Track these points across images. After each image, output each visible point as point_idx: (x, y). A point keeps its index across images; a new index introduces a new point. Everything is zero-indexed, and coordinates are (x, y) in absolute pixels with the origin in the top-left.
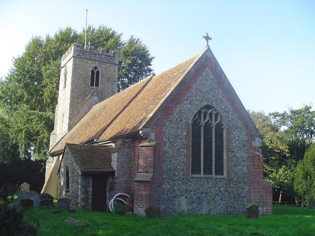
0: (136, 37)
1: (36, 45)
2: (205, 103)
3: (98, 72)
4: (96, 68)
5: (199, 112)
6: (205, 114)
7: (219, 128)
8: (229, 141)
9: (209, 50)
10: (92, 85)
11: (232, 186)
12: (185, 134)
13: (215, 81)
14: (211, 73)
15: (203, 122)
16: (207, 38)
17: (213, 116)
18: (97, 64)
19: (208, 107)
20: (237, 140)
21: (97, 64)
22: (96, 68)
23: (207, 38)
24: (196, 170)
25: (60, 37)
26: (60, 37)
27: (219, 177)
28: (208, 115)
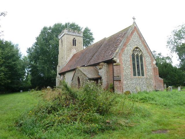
0: (89, 28)
1: (45, 31)
2: (136, 46)
3: (75, 40)
4: (74, 39)
5: (134, 50)
6: (136, 51)
7: (141, 56)
8: (145, 62)
9: (134, 23)
10: (73, 45)
11: (148, 81)
12: (130, 59)
13: (138, 37)
14: (137, 34)
15: (136, 54)
16: (134, 19)
17: (139, 52)
18: (74, 37)
19: (137, 48)
20: (148, 61)
21: (74, 37)
22: (74, 39)
23: (134, 19)
24: (135, 75)
25: (17, 62)
26: (17, 62)
27: (135, 77)
28: (137, 51)
